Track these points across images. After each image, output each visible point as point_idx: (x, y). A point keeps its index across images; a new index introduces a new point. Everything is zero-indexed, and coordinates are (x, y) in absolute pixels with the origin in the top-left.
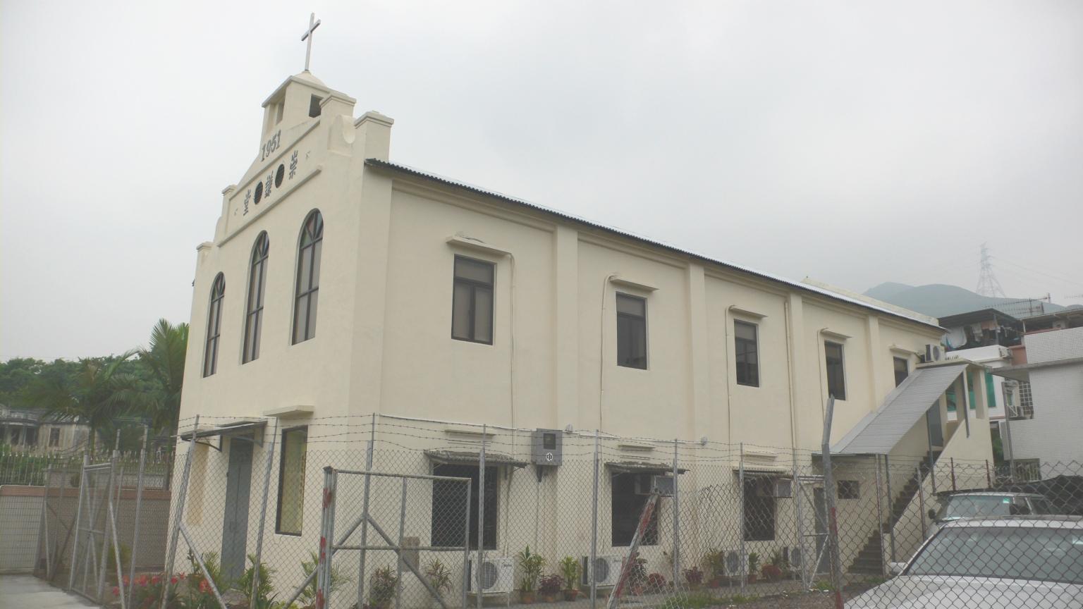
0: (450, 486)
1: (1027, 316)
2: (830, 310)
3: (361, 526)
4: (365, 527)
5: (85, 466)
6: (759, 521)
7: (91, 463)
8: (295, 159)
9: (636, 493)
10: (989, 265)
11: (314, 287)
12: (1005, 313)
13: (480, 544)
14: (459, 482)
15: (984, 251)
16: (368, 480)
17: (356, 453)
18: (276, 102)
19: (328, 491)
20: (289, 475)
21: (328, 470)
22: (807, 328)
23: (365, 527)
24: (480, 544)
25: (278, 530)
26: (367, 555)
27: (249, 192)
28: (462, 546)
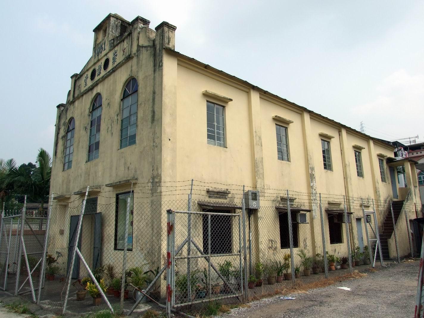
0: (225, 219)
1: (409, 144)
2: (354, 136)
3: (186, 246)
4: (189, 244)
5: (3, 217)
6: (288, 234)
7: (5, 216)
8: (116, 54)
9: (289, 220)
10: (364, 130)
11: (70, 160)
12: (402, 143)
13: (210, 251)
14: (227, 216)
15: (361, 125)
16: (189, 216)
17: (178, 202)
18: (100, 29)
19: (171, 224)
20: (120, 217)
21: (169, 212)
22: (349, 142)
23: (189, 244)
24: (210, 251)
25: (116, 248)
26: (191, 262)
27: (87, 75)
28: (230, 253)
